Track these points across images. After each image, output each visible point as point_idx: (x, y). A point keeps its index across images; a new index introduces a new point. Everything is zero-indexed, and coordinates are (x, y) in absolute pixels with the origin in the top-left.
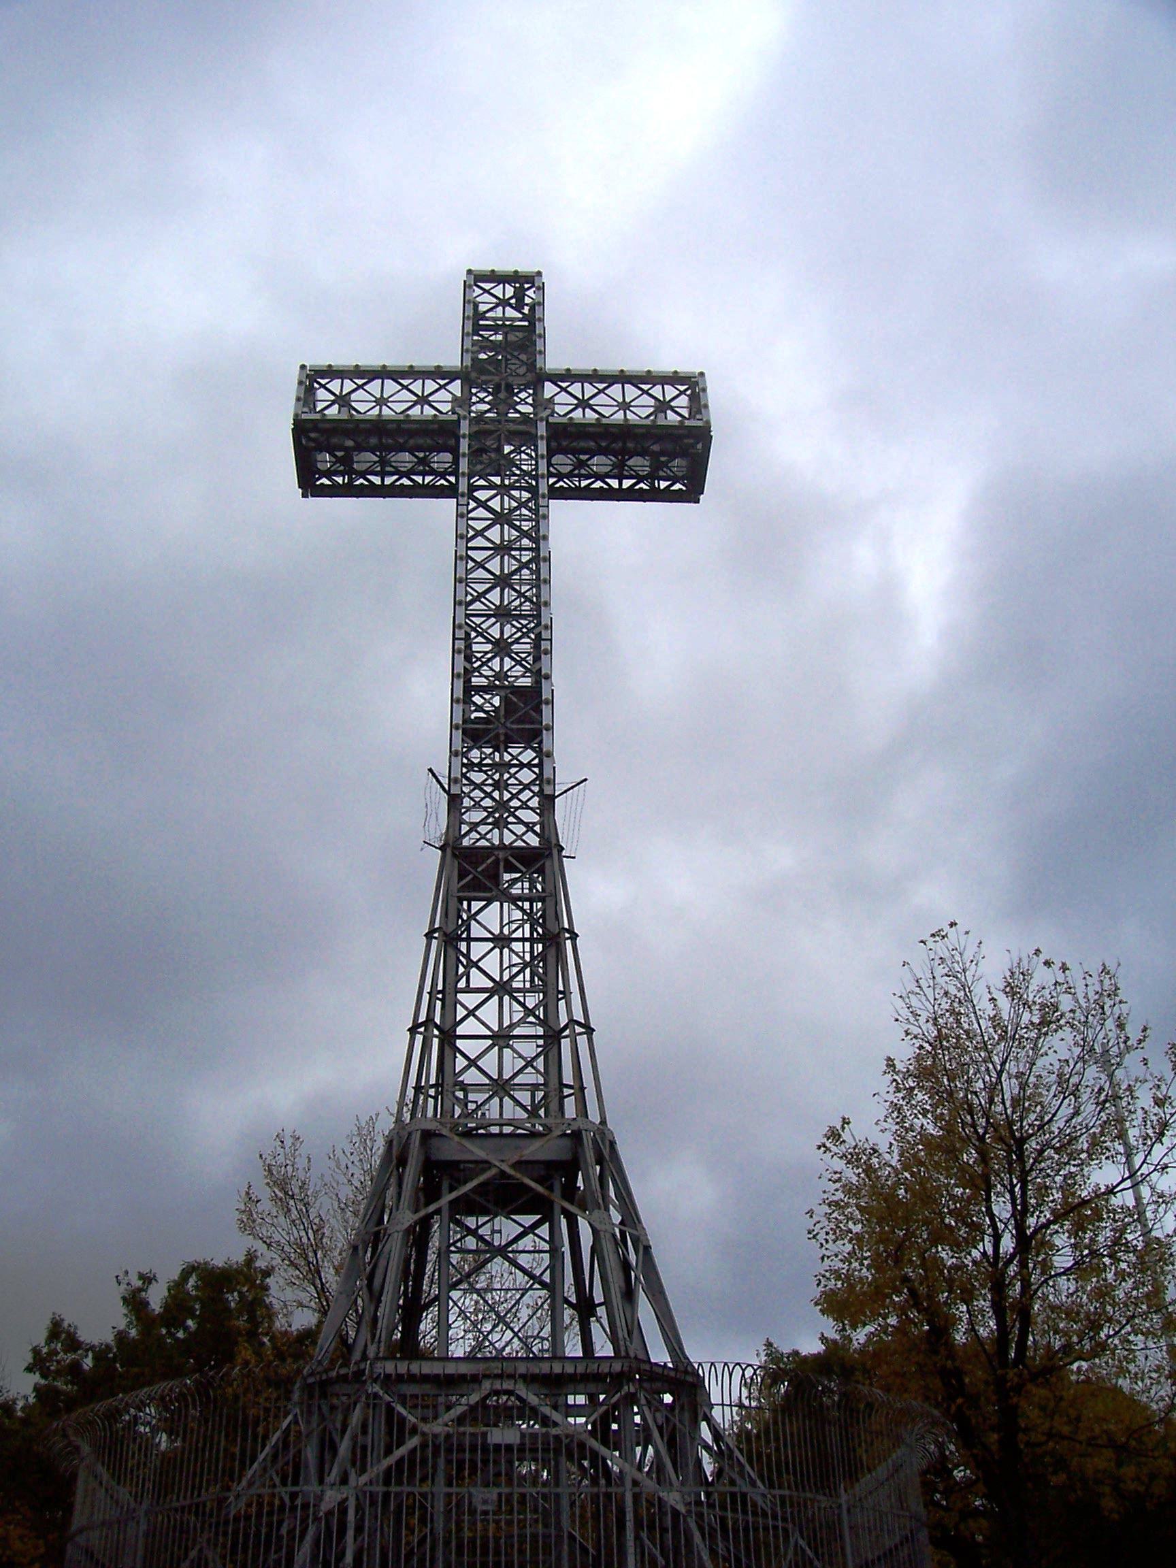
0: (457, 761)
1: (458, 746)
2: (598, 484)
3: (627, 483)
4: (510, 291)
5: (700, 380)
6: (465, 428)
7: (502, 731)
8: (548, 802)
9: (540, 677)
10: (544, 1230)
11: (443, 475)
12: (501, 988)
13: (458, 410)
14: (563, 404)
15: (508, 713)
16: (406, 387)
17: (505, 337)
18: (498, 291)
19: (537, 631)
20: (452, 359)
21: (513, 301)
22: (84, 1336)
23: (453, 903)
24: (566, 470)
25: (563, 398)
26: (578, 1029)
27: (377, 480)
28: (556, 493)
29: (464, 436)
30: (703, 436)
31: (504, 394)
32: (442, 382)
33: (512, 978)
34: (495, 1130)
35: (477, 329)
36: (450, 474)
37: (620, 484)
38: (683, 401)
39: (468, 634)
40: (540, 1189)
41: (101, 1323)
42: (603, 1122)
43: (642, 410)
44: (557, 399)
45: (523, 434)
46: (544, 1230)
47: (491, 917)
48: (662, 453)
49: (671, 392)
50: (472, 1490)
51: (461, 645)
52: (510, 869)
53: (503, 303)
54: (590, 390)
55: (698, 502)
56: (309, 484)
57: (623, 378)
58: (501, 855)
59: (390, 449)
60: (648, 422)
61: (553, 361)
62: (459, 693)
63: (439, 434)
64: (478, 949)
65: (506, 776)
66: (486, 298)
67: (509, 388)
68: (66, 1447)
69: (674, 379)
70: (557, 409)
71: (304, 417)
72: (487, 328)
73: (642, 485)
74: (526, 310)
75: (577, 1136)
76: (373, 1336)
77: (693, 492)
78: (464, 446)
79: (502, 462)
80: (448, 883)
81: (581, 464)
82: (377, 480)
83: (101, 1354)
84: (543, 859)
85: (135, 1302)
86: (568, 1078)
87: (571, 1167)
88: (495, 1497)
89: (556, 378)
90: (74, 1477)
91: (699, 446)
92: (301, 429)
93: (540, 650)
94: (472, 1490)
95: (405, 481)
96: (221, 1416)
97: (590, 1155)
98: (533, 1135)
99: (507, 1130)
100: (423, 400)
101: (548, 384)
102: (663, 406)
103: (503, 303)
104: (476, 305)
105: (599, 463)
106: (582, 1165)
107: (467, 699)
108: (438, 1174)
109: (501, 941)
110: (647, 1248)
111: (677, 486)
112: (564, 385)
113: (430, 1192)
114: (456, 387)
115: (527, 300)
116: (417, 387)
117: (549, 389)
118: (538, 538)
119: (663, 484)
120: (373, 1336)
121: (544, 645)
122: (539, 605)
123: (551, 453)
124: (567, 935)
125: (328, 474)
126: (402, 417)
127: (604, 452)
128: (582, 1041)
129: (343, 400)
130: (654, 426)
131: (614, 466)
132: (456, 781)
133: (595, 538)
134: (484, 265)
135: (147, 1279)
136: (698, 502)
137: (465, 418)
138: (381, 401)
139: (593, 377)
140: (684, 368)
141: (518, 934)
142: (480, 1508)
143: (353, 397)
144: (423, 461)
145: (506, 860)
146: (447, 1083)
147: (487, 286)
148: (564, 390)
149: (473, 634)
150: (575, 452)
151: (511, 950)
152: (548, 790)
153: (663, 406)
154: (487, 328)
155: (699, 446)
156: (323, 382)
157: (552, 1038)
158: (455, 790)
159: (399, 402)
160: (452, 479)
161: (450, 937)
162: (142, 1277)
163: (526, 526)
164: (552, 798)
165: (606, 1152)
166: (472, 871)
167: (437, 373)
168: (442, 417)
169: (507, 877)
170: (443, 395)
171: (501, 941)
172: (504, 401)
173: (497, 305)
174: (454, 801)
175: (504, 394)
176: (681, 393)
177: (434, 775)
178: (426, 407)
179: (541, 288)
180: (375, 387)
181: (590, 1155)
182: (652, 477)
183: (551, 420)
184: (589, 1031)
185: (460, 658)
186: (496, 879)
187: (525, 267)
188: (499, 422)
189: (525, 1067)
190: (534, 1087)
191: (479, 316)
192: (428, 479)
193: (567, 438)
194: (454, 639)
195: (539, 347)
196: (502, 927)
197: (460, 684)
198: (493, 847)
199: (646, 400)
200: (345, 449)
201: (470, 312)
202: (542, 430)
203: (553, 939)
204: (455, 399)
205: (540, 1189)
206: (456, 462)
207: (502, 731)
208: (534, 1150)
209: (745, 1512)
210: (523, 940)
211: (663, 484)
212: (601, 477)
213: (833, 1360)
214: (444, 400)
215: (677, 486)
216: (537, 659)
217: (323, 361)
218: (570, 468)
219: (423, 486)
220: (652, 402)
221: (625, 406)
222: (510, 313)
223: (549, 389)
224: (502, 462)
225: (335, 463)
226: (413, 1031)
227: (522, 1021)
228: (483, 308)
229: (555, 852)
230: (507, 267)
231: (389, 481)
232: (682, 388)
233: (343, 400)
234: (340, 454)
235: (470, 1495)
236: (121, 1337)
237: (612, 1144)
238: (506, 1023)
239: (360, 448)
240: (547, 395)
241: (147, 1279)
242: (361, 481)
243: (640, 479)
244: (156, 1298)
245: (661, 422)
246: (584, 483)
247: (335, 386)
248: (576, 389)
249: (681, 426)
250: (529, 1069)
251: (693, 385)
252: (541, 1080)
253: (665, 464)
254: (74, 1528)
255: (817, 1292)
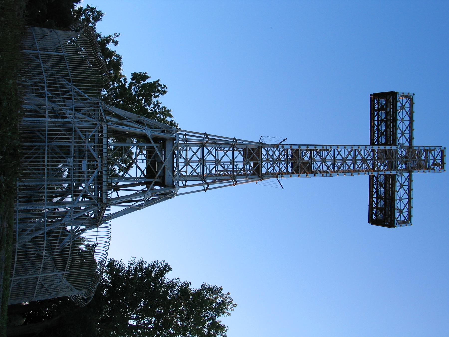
0: (288, 147)
1: (294, 147)
2: (374, 190)
3: (375, 200)
4: (439, 161)
5: (410, 224)
6: (394, 148)
7: (298, 161)
8: (276, 175)
9: (315, 173)
10: (142, 176)
11: (378, 140)
12: (217, 162)
13: (400, 145)
14: (401, 179)
15: (303, 163)
16: (407, 128)
17: (423, 160)
18: (439, 157)
19: (329, 172)
20: (415, 143)
21: (435, 162)
22: (98, 23)
23: (244, 147)
24: (379, 180)
25: (403, 179)
26: (206, 187)
27: (376, 119)
28: (371, 178)
29: (391, 147)
30: (391, 225)
31: (405, 159)
32: (408, 140)
33: (221, 165)
34: (175, 160)
35: (426, 151)
36: (378, 143)
37: (375, 198)
38: (402, 219)
39: (328, 150)
40: (158, 176)
41: (102, 29)
42: (177, 195)
43: (399, 205)
44: (403, 177)
45: (392, 166)
46: (142, 176)
47: (240, 158)
48: (385, 212)
49: (406, 214)
50: (73, 158)
51: (325, 147)
52: (255, 164)
53: (435, 159)
54: (406, 188)
55: (369, 223)
56: (376, 96)
57: (410, 199)
58: (259, 162)
59: (386, 123)
60: (396, 207)
61: (416, 175)
62: (310, 147)
63: (392, 139)
64: (230, 154)
65: (283, 163)
66: (436, 154)
67: (406, 162)
68: (80, 27)
69: (410, 216)
70: (400, 177)
71: (398, 95)
72: (426, 154)
73: (374, 205)
74: (432, 167)
75: (174, 187)
76: (114, 124)
77: (372, 221)
78: (388, 148)
79: (383, 160)
80: (251, 144)
81: (382, 186)
82: (376, 119)
83: (93, 29)
84: (257, 174)
85: (108, 40)
86: (189, 183)
87: (162, 184)
88: (71, 165)
89: (410, 177)
90: (69, 30)
91: (388, 224)
92: (393, 94)
93: (323, 173)
94: (73, 158)
95: (376, 128)
96: (95, 78)
97: (168, 191)
98: (173, 172)
99: (175, 164)
100: (403, 134)
101: (408, 174)
102: (401, 212)
103: (435, 159)
104: (434, 150)
105: (382, 191)
106: (165, 188)
107: (307, 150)
108: (162, 143)
109: (233, 162)
110: (138, 209)
111: (374, 216)
112: (408, 179)
113: (156, 139)
114: (407, 144)
115: (435, 167)
116: (407, 132)
117: (406, 175)
118: (358, 172)
119: (374, 212)
120: (114, 124)
121: (325, 174)
122: (337, 172)
123: (385, 176)
124: (235, 183)
125: (378, 103)
126: (397, 127)
127: (385, 193)
128: (201, 188)
129: (403, 107)
130: (394, 209)
131: (380, 196)
132: (283, 147)
133: (356, 189)
134: (446, 152)
135: (116, 43)
136: (369, 223)
137: (397, 147)
138: (402, 120)
139: (410, 189)
140: (413, 219)
141: (235, 167)
142: (67, 160)
143: (404, 111)
144: (382, 134)
145: (258, 163)
146: (187, 144)
147: (440, 154)
148: (406, 179)
149: (328, 152)
150: (385, 183)
151: (215, 157)
152: (280, 176)
153: (401, 212)
154: (426, 154)
155: (388, 224)
156: (409, 101)
157: (202, 178)
158: (280, 147)
159: (402, 126)
160: (376, 143)
161: (234, 144)
162: (117, 41)
163: (362, 169)
164: (277, 177)
165: (168, 196)
166: (253, 152)
167: (411, 139)
168: (397, 140)
169: (251, 163)
170: (404, 140)
171: (233, 162)
172: (402, 160)
173: (434, 157)
174: (276, 146)
175: (405, 159)
176: (405, 218)
177: (284, 140)
178: (401, 135)
179: (439, 171)
180: (407, 118)
181: (168, 191)
182: (377, 208)
183: (396, 176)
184: (205, 190)
185: (320, 147)
186: (252, 160)
187: (446, 166)
188: (396, 159)
189: (192, 168)
190: (186, 172)
191: (430, 151)
192: (376, 135)
193: (390, 181)
194: (327, 145)
195: (420, 171)
196: (237, 162)
197: (313, 147)
198: (262, 159)
199: (403, 206)
200: (386, 109)
201: (432, 148)
202: (393, 173)
203: (232, 177)
204: (403, 144)
205: (158, 176)
206: (382, 145)
207: (298, 161)
208: (168, 173)
209: (60, 240)
210: (233, 168)
211: (374, 212)
212: (377, 190)
213: (93, 263)
214: (403, 140)
215: (374, 216)
216: (320, 172)
217: (415, 100)
218: (380, 181)
219: (374, 133)
220: (402, 208)
221: (401, 200)
222: (431, 162)
223: (406, 175)
224: (383, 160)
225: (381, 105)
226: (205, 134)
227: (207, 169)
228: (433, 152)
229: (260, 179)
230: (446, 159)
231: (376, 122)
232: (407, 218)
233: (403, 107)
234: (385, 106)
235: (71, 157)
236: (98, 35)
237: (171, 198)
238: (206, 163)
239: (387, 114)
240: (404, 174)
241: (116, 43)
242: (376, 114)
243: (376, 204)
244: (111, 47)
245: (396, 211)
246: (375, 186)
247: (407, 105)
248: (406, 183)
249: (394, 218)
250: (192, 170)
251: (408, 221)
252: (188, 174)
253: (381, 212)
254: (57, 31)
255: (224, 291)
